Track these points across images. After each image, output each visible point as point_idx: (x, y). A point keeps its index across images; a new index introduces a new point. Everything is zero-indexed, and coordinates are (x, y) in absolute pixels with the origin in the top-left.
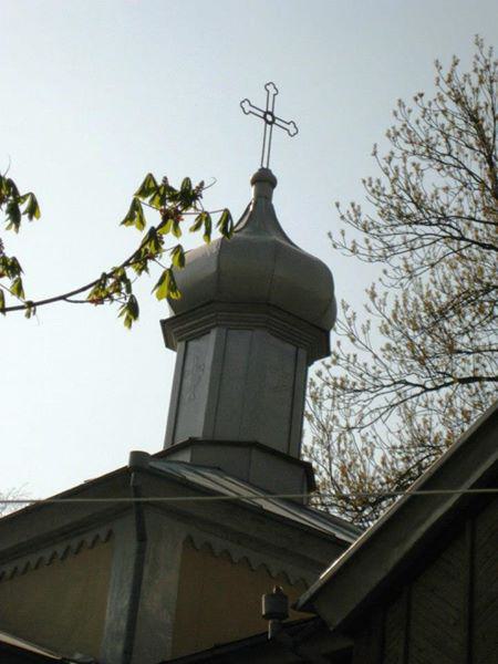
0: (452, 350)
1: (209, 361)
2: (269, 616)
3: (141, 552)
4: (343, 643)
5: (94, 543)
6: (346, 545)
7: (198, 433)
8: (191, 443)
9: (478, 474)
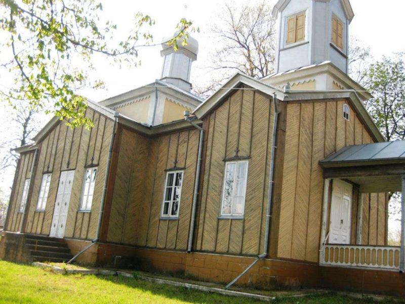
0: (221, 61)
1: (170, 60)
2: (185, 115)
3: (156, 101)
4: (201, 122)
5: (293, 85)
6: (202, 102)
7: (168, 76)
8: (166, 78)
9: (234, 86)
